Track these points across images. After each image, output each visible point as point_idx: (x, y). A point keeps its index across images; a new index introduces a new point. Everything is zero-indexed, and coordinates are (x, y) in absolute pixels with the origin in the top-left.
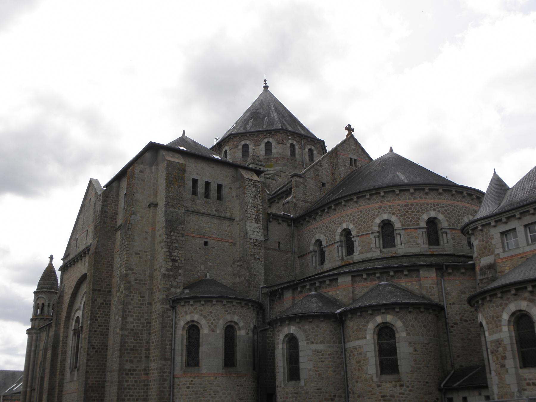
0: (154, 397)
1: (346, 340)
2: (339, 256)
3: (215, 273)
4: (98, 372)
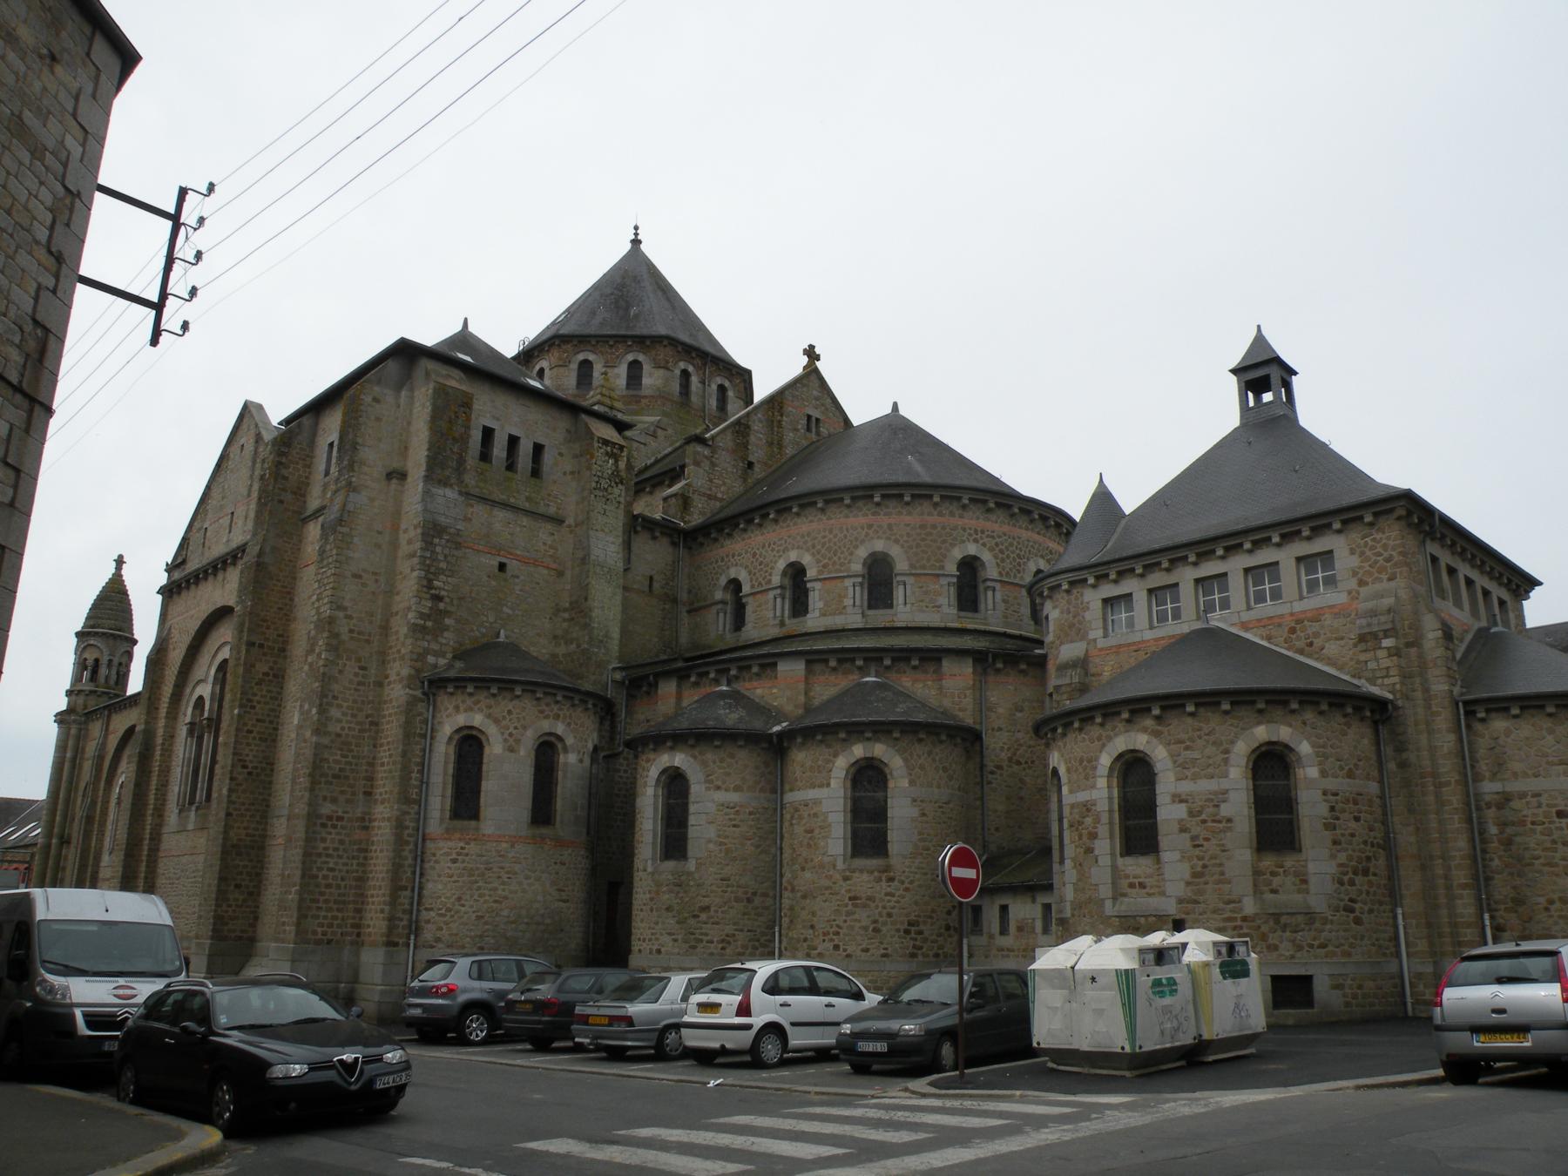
0: (381, 876)
1: (787, 787)
2: (775, 617)
4: (251, 816)
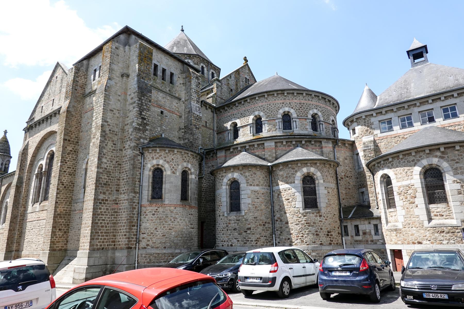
0: (124, 222)
4: (65, 203)
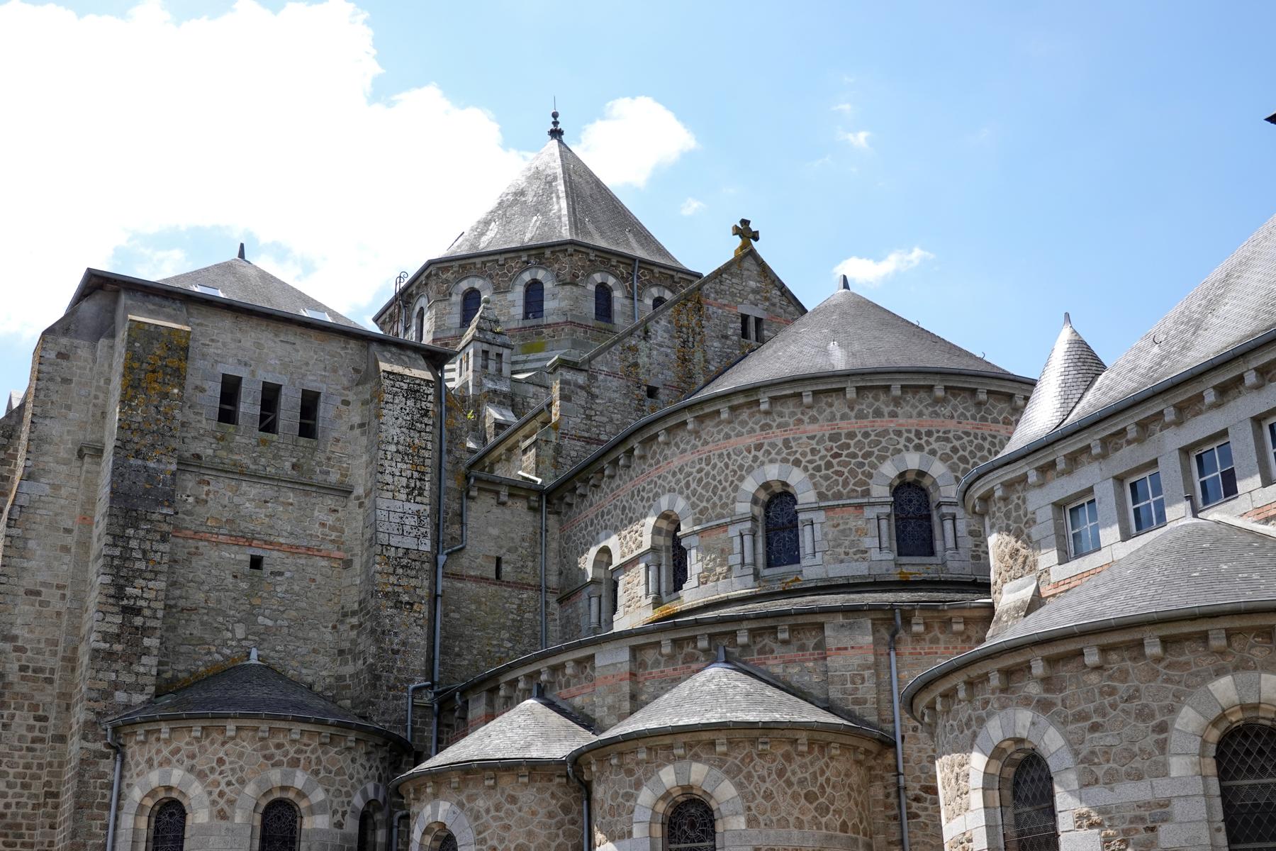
3: (278, 648)
